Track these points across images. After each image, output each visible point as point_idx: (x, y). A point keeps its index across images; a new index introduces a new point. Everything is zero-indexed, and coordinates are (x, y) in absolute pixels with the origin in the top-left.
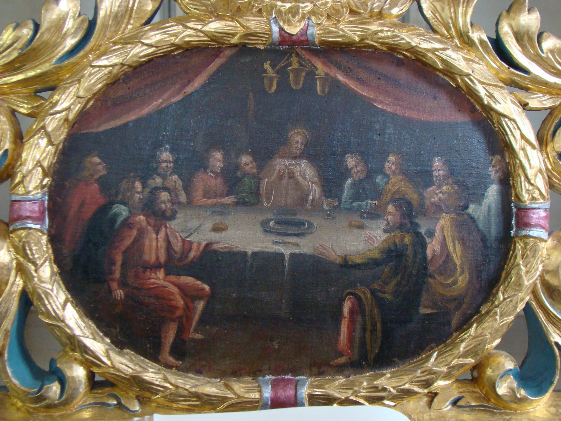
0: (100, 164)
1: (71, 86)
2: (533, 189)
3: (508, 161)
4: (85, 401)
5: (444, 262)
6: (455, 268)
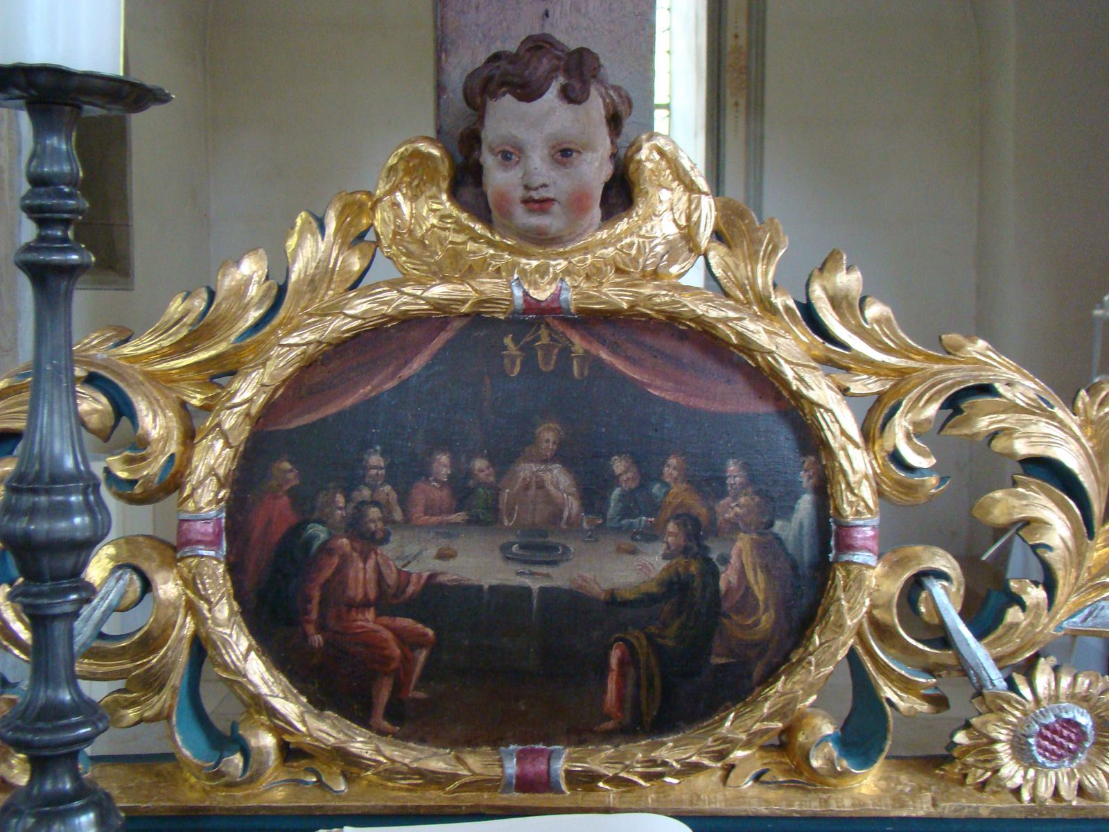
0: (291, 471)
1: (254, 371)
2: (858, 501)
3: (824, 462)
4: (276, 778)
5: (742, 597)
6: (757, 605)
